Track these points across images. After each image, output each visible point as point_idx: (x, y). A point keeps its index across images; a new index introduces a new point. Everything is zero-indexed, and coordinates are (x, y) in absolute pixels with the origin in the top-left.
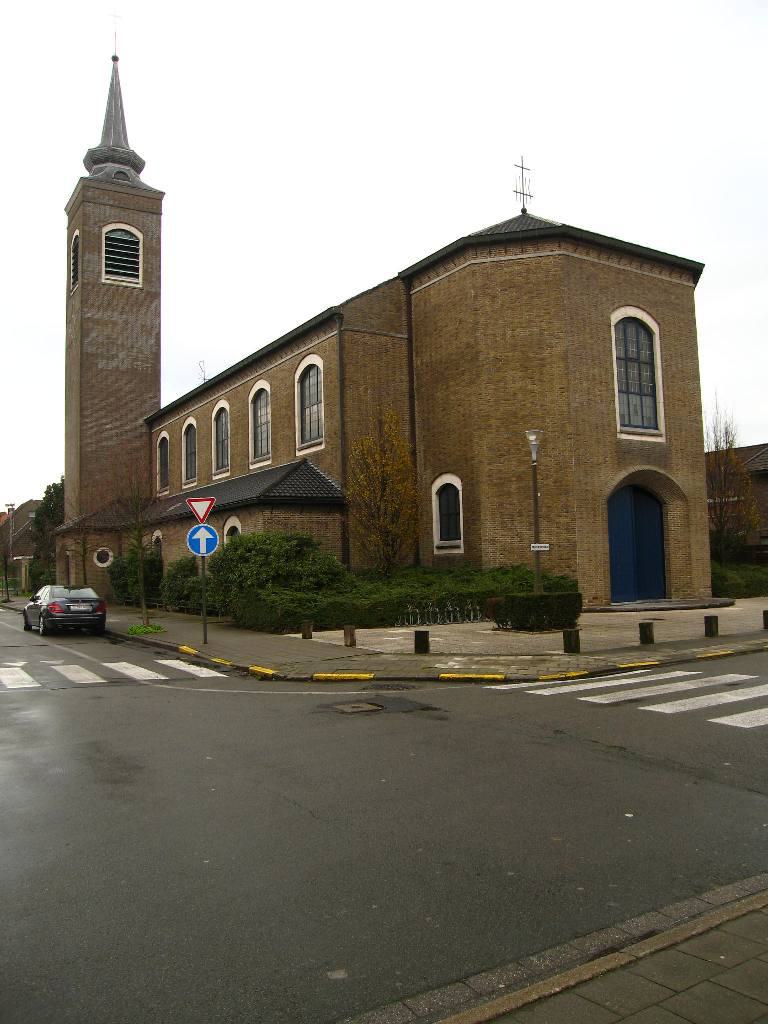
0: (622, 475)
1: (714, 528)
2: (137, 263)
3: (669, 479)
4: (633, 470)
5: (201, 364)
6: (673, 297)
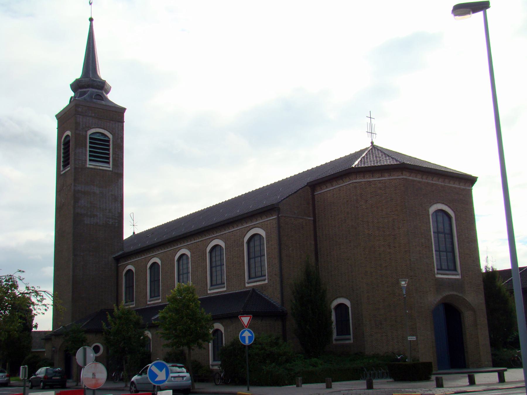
0: (439, 298)
1: (471, 13)
2: (109, 154)
3: (464, 299)
4: (445, 295)
5: (132, 215)
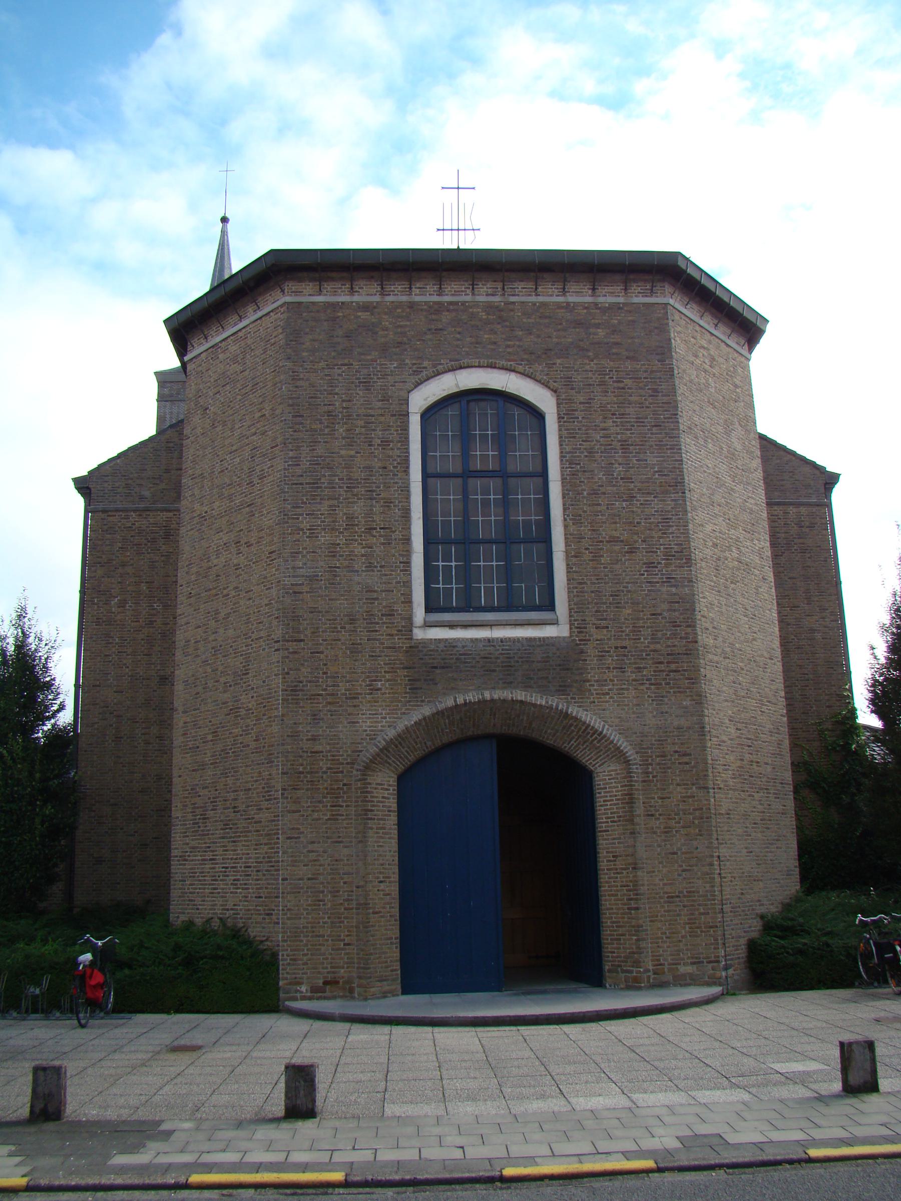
6: (601, 333)
